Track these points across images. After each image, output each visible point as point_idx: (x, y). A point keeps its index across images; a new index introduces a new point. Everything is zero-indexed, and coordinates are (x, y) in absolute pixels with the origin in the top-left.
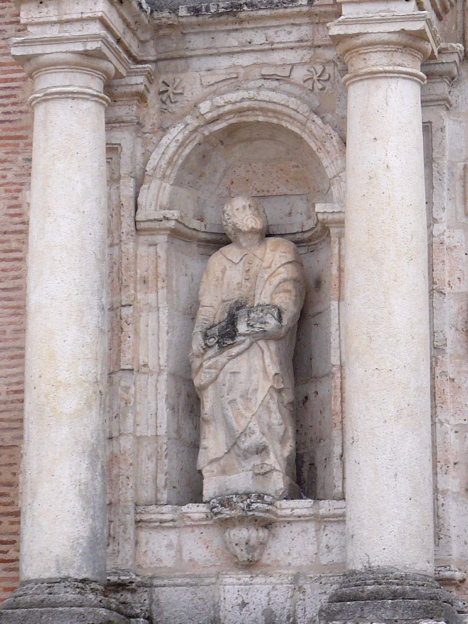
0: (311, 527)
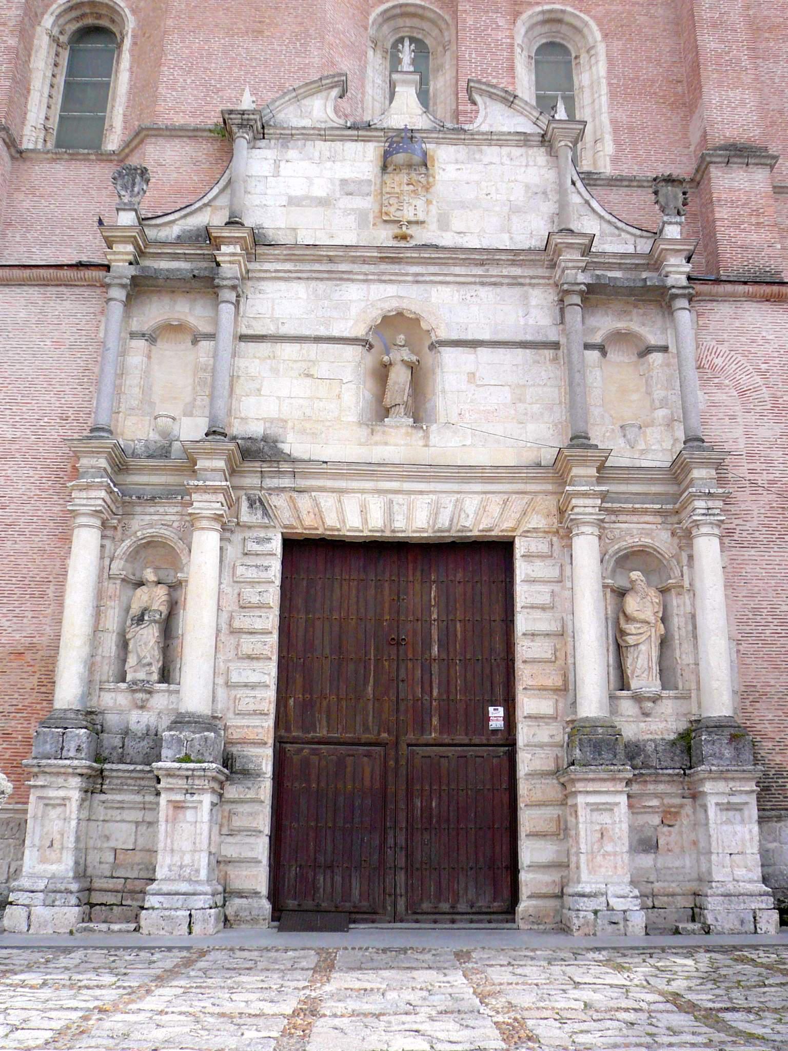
0: (167, 694)
